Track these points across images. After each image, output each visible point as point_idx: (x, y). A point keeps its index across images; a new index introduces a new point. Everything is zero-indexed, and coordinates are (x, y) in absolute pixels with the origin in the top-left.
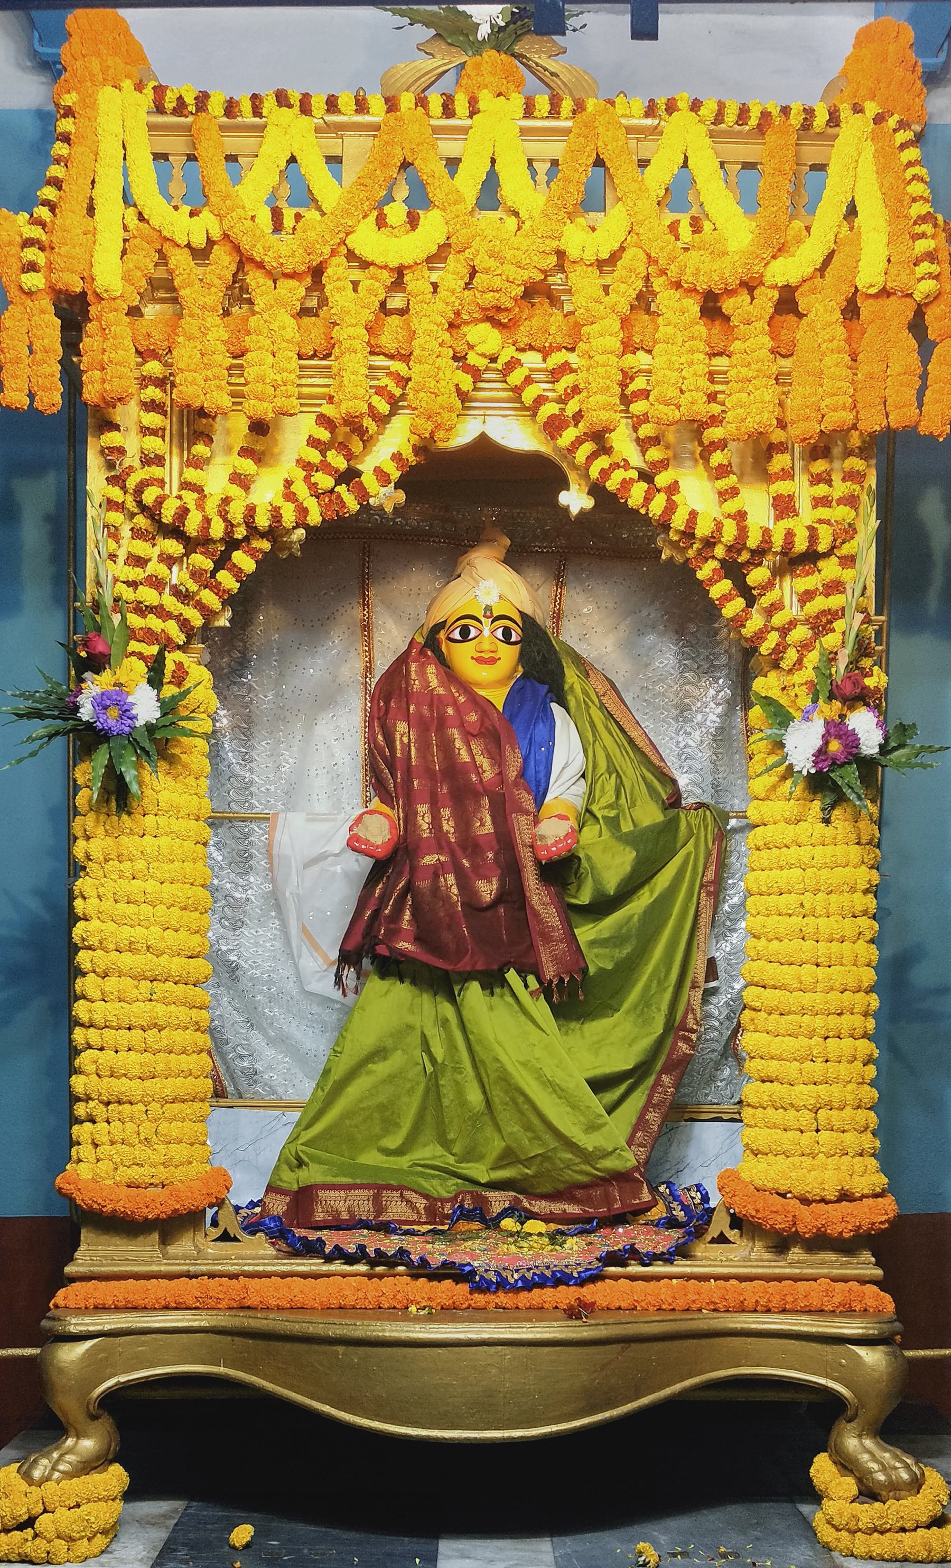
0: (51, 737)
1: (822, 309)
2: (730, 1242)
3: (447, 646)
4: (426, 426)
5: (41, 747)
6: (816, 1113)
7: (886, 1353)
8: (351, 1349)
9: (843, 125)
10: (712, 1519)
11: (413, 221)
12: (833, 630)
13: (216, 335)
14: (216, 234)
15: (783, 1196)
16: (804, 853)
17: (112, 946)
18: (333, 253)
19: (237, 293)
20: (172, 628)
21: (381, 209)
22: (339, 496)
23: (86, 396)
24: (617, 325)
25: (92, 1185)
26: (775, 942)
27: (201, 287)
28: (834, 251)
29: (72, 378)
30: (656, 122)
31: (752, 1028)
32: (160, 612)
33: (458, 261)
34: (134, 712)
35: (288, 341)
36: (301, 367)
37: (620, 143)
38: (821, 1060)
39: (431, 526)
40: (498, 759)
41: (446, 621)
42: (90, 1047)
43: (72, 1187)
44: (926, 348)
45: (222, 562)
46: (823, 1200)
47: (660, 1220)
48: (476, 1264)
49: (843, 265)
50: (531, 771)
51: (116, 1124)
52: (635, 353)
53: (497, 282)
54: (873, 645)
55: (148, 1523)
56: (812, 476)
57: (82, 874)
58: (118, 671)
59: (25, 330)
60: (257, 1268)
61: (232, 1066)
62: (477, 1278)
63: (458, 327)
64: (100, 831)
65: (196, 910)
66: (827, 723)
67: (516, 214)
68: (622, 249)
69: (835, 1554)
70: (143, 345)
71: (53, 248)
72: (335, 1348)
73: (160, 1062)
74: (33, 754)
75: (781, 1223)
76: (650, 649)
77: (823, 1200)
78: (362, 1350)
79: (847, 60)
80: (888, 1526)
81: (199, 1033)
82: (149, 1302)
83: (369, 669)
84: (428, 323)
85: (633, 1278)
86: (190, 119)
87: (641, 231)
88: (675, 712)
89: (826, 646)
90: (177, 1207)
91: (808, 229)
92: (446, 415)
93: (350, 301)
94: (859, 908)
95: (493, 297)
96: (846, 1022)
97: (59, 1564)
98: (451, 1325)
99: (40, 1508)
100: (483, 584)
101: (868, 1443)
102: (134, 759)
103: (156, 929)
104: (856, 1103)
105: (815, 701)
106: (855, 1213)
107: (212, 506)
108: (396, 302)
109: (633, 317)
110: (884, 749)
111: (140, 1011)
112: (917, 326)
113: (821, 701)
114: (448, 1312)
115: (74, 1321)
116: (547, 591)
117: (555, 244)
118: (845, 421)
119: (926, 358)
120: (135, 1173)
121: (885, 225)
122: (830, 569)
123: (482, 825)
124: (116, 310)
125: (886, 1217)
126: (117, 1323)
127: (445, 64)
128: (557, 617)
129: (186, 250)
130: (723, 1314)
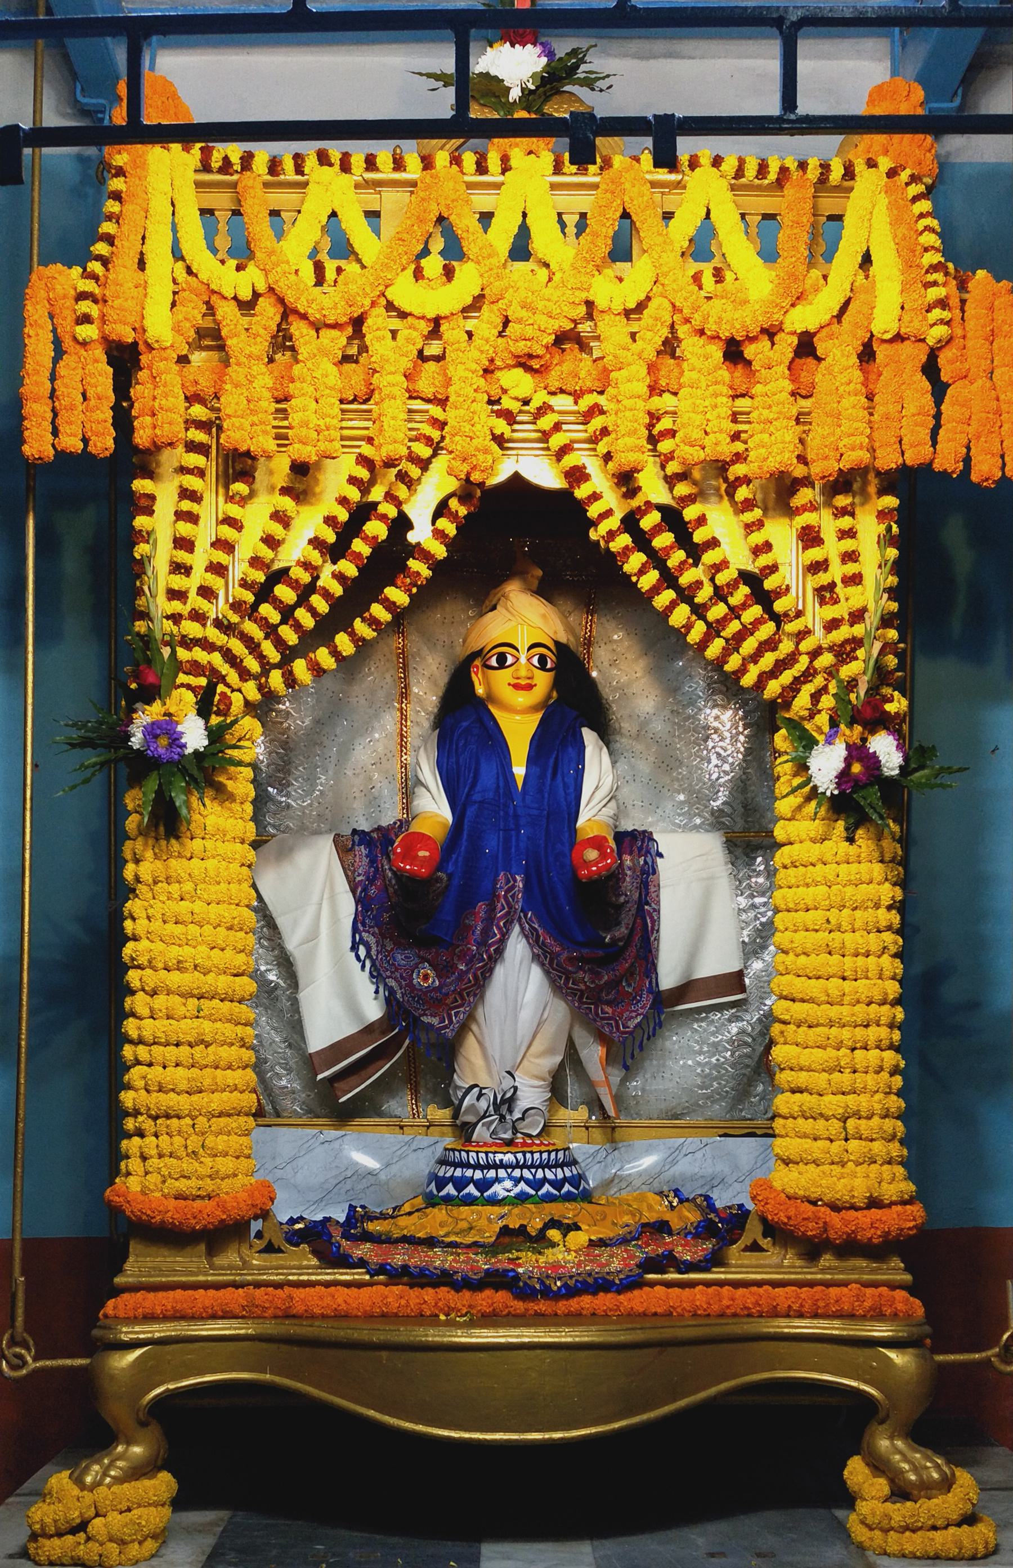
1: (839, 354)
5: (93, 774)
6: (845, 1122)
7: (917, 1356)
9: (857, 178)
10: (749, 1524)
11: (449, 273)
12: (856, 658)
13: (262, 383)
14: (261, 288)
15: (814, 1203)
17: (160, 965)
19: (282, 341)
24: (644, 371)
26: (803, 957)
27: (248, 338)
28: (850, 298)
29: (123, 420)
31: (782, 1040)
32: (208, 646)
33: (491, 311)
34: (183, 741)
35: (331, 388)
41: (482, 649)
46: (854, 1207)
48: (521, 1270)
53: (529, 332)
58: (168, 701)
60: (302, 1278)
63: (492, 372)
64: (149, 854)
65: (241, 929)
66: (849, 747)
67: (547, 265)
68: (648, 298)
69: (869, 1553)
72: (377, 1353)
73: (207, 1077)
75: (812, 1230)
76: (679, 673)
77: (854, 1207)
81: (244, 1050)
86: (235, 177)
91: (825, 277)
92: (481, 457)
93: (389, 349)
94: (883, 924)
96: (874, 1033)
99: (92, 1512)
101: (899, 1443)
103: (203, 949)
108: (433, 349)
111: (187, 1029)
112: (931, 369)
113: (842, 726)
114: (490, 1319)
115: (124, 1329)
117: (584, 295)
120: (182, 1185)
121: (898, 273)
124: (166, 359)
126: (166, 1333)
128: (588, 643)
129: (233, 303)
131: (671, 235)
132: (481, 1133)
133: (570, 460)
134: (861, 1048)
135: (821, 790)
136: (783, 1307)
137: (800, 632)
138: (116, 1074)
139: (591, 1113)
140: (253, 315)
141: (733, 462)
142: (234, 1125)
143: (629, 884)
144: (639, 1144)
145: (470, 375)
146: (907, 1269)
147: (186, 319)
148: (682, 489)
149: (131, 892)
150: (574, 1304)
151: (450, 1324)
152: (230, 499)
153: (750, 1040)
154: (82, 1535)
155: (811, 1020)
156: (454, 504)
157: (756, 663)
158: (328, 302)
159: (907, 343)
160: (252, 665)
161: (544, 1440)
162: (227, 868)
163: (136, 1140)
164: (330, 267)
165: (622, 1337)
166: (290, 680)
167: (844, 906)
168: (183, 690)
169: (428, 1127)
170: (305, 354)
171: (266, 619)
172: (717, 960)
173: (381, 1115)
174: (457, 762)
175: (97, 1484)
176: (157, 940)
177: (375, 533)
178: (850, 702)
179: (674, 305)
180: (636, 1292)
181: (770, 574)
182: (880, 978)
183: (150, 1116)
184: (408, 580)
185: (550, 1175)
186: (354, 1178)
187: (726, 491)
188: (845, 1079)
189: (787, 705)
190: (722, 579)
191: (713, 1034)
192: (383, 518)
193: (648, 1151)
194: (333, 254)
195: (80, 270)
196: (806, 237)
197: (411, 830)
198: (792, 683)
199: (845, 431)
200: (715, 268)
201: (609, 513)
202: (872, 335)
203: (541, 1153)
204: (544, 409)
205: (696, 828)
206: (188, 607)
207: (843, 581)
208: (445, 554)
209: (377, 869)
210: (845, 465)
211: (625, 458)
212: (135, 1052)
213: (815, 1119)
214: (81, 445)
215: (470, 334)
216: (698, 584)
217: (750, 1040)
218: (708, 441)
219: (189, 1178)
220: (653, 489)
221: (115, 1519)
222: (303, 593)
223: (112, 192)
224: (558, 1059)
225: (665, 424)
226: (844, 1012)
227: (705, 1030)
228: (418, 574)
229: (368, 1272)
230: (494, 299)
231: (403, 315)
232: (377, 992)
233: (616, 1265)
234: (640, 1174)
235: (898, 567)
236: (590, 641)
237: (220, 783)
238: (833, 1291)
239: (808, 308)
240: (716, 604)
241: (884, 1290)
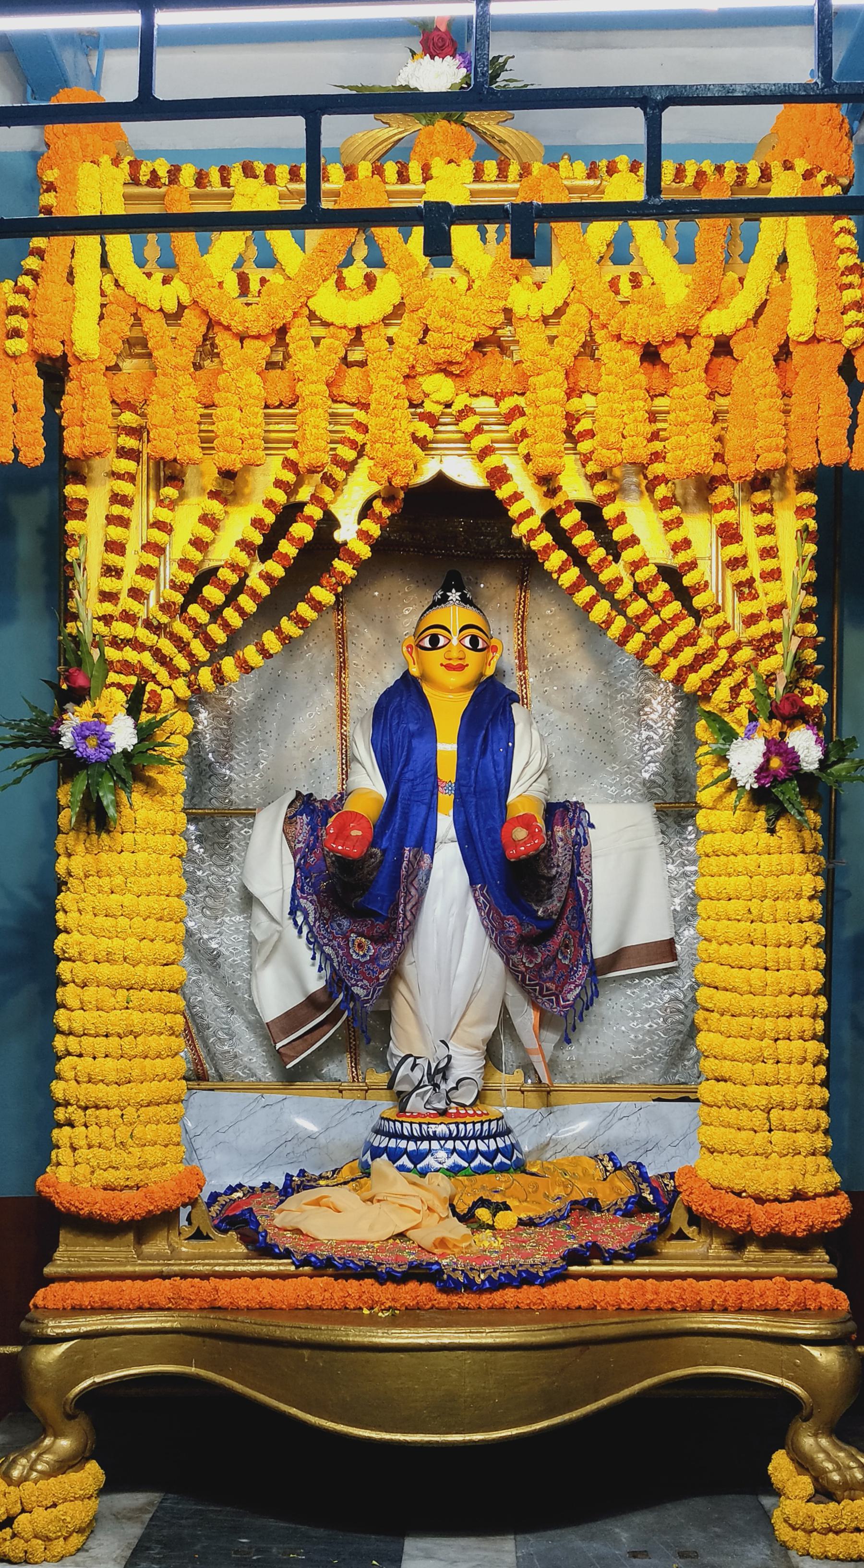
0: (35, 764)
1: (755, 357)
2: (688, 1238)
4: (382, 474)
5: (24, 774)
6: (768, 1113)
7: (841, 1354)
8: (317, 1353)
9: (774, 180)
10: (675, 1514)
11: (370, 282)
12: (776, 653)
13: (187, 393)
14: (186, 300)
15: (739, 1194)
16: (750, 861)
17: (90, 958)
18: (295, 315)
19: (207, 348)
21: (340, 273)
23: (67, 450)
24: (561, 377)
25: (70, 1189)
26: (725, 946)
27: (174, 348)
28: (766, 300)
29: (54, 429)
30: (598, 182)
32: (137, 645)
33: (412, 320)
34: (111, 741)
35: (255, 398)
36: (267, 416)
39: (401, 537)
42: (69, 1054)
43: (51, 1190)
44: (856, 390)
46: (777, 1200)
47: (630, 1198)
48: (444, 1262)
49: (775, 315)
51: (93, 1128)
52: (580, 397)
53: (448, 340)
55: (124, 1517)
56: (755, 506)
57: (63, 888)
58: (97, 702)
59: (9, 390)
60: (227, 1269)
61: (213, 1050)
62: (445, 1276)
63: (414, 377)
64: (80, 848)
65: (171, 919)
66: (767, 742)
67: (467, 272)
68: (566, 304)
69: (792, 1553)
70: (121, 398)
74: (17, 781)
77: (777, 1200)
78: (327, 1355)
79: (778, 118)
80: (843, 1527)
81: (173, 1038)
82: (124, 1302)
84: (384, 379)
85: (593, 1277)
86: (164, 189)
87: (583, 289)
90: (151, 1208)
91: (741, 280)
92: (402, 463)
93: (310, 360)
94: (805, 914)
95: (445, 353)
97: (36, 1563)
98: (413, 1330)
99: (18, 1508)
101: (824, 1442)
102: (112, 784)
103: (132, 940)
104: (807, 1103)
106: (808, 1212)
108: (356, 355)
109: (578, 363)
110: (824, 764)
111: (116, 1019)
112: (847, 369)
113: (761, 721)
114: (411, 1316)
115: (51, 1324)
117: (502, 304)
119: (855, 399)
120: (111, 1176)
121: (813, 277)
124: (94, 371)
125: (838, 1216)
126: (94, 1322)
127: (400, 133)
129: (160, 314)
131: (588, 241)
132: (415, 1103)
133: (492, 461)
134: (784, 1039)
135: (740, 784)
136: (706, 1302)
137: (718, 628)
138: (47, 1062)
139: (526, 1076)
140: (180, 325)
141: (651, 462)
142: (163, 1114)
143: (561, 855)
144: (574, 1108)
145: (391, 382)
146: (832, 1261)
147: (115, 332)
148: (602, 488)
149: (60, 885)
150: (498, 1297)
151: (373, 1322)
152: (160, 503)
153: (682, 1007)
155: (733, 1010)
156: (377, 505)
157: (675, 657)
158: (254, 317)
159: (822, 343)
160: (182, 663)
161: (464, 1442)
162: (158, 860)
164: (254, 276)
165: (544, 1337)
166: (219, 678)
167: (766, 897)
168: (114, 689)
169: (367, 1091)
170: (230, 364)
171: (194, 619)
172: (649, 929)
173: (321, 1077)
174: (391, 740)
175: (24, 1479)
176: (87, 932)
177: (301, 535)
178: (769, 696)
179: (591, 311)
180: (560, 1285)
181: (689, 571)
182: (803, 969)
183: (80, 1107)
184: (334, 580)
185: (482, 1147)
186: (295, 1141)
187: (646, 487)
189: (707, 698)
190: (642, 575)
191: (646, 1000)
192: (309, 519)
193: (582, 1116)
194: (260, 264)
195: (12, 283)
196: (722, 241)
197: (345, 809)
198: (712, 677)
199: (761, 434)
200: (632, 274)
201: (530, 512)
202: (788, 337)
203: (474, 1123)
204: (467, 412)
205: (629, 799)
206: (120, 608)
207: (761, 577)
208: (369, 554)
209: (317, 838)
210: (761, 466)
211: (545, 464)
212: (65, 1043)
213: (739, 1109)
214: (12, 456)
215: (390, 341)
216: (619, 581)
217: (682, 1007)
218: (625, 444)
219: (117, 1169)
220: (575, 486)
221: (40, 1515)
222: (232, 592)
223: (43, 207)
224: (493, 1027)
225: (585, 424)
227: (638, 997)
228: (343, 573)
229: (293, 1263)
230: (413, 308)
231: (326, 324)
232: (314, 958)
233: (538, 1258)
234: (575, 1138)
235: (817, 562)
237: (150, 777)
238: (758, 1284)
239: (724, 312)
240: (636, 600)
241: (807, 1283)
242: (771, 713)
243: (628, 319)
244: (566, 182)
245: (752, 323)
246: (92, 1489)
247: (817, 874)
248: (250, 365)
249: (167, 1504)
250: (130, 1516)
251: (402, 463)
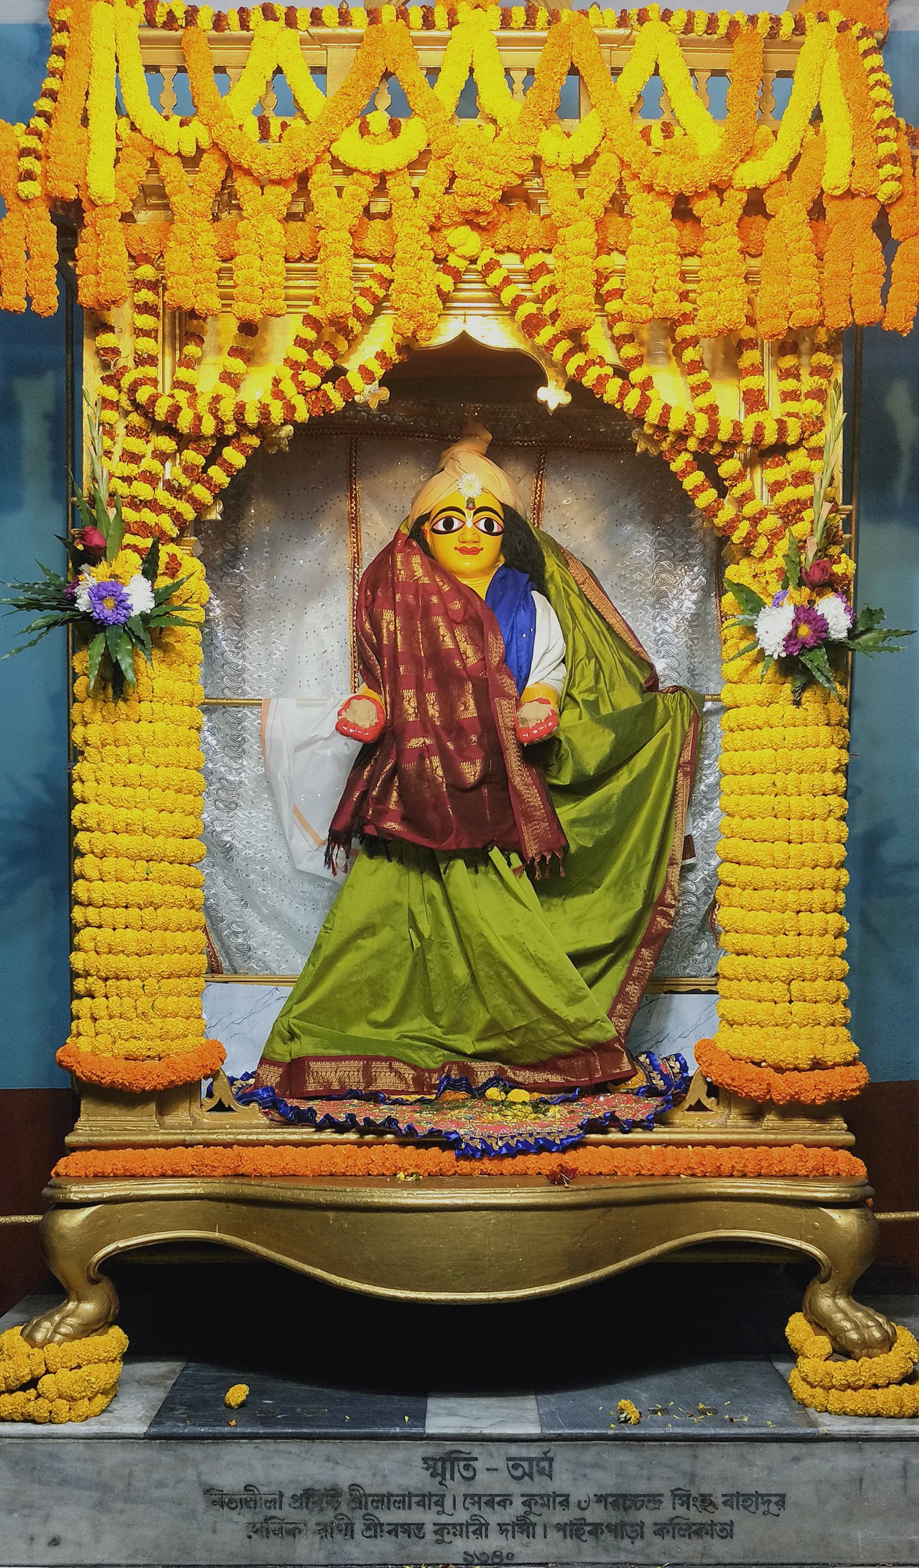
0: (49, 626)
1: (789, 210)
3: (432, 537)
5: (40, 636)
7: (859, 1217)
8: (342, 1214)
10: (691, 1377)
11: (395, 129)
12: (802, 519)
13: (206, 240)
14: (205, 143)
15: (758, 1064)
16: (776, 734)
17: (109, 828)
18: (318, 160)
19: (226, 199)
20: (166, 522)
22: (325, 394)
24: (592, 227)
25: (91, 1058)
26: (748, 819)
27: (192, 194)
28: (800, 154)
29: (68, 281)
31: (727, 903)
32: (154, 506)
33: (438, 167)
34: (129, 602)
35: (275, 245)
36: (288, 270)
37: (594, 52)
38: (793, 933)
40: (481, 647)
42: (88, 925)
45: (214, 458)
46: (796, 1069)
47: (640, 1088)
48: (461, 1132)
49: (810, 168)
50: (513, 657)
53: (476, 187)
54: (841, 533)
55: (147, 1383)
57: (80, 758)
58: (114, 563)
60: (251, 1137)
62: (463, 1146)
63: (439, 230)
64: (98, 717)
65: (190, 793)
66: (797, 609)
67: (494, 121)
68: (596, 154)
70: (136, 250)
71: (49, 158)
73: (157, 939)
74: (33, 643)
77: (796, 1069)
80: (861, 1383)
81: (193, 911)
82: (147, 1170)
83: (356, 560)
84: (410, 226)
85: (613, 1144)
86: (180, 32)
87: (614, 137)
88: (652, 599)
89: (795, 534)
90: (174, 1078)
91: (775, 133)
92: (428, 315)
94: (829, 787)
95: (473, 201)
97: (61, 1423)
98: (438, 1191)
99: (42, 1369)
100: (466, 477)
101: (842, 1302)
102: (130, 647)
103: (152, 811)
105: (785, 587)
106: (827, 1080)
107: (203, 404)
108: (379, 207)
109: (607, 219)
110: (852, 633)
111: (136, 891)
112: (881, 226)
113: (791, 588)
114: (436, 1179)
115: (74, 1189)
116: (528, 483)
117: (531, 150)
118: (811, 318)
120: (133, 1046)
121: (849, 128)
122: (799, 460)
123: (466, 709)
124: (109, 216)
125: (857, 1085)
126: (116, 1191)
128: (538, 508)
129: (177, 159)
130: (701, 1180)
135: (767, 653)
146: (850, 1130)
149: (75, 754)
154: (32, 1391)
162: (176, 731)
163: (87, 1000)
170: (250, 211)
176: (106, 802)
178: (800, 563)
180: (581, 1151)
188: (791, 940)
202: (822, 192)
210: (794, 323)
213: (759, 981)
214: (25, 304)
218: (656, 299)
221: (64, 1376)
223: (55, 48)
225: (614, 283)
226: (790, 875)
236: (539, 505)
242: (800, 578)
243: (661, 168)
244: (597, 31)
245: (785, 176)
246: (116, 1352)
247: (841, 747)
248: (271, 212)
249: (189, 1371)
250: (151, 1382)
251: (428, 315)
